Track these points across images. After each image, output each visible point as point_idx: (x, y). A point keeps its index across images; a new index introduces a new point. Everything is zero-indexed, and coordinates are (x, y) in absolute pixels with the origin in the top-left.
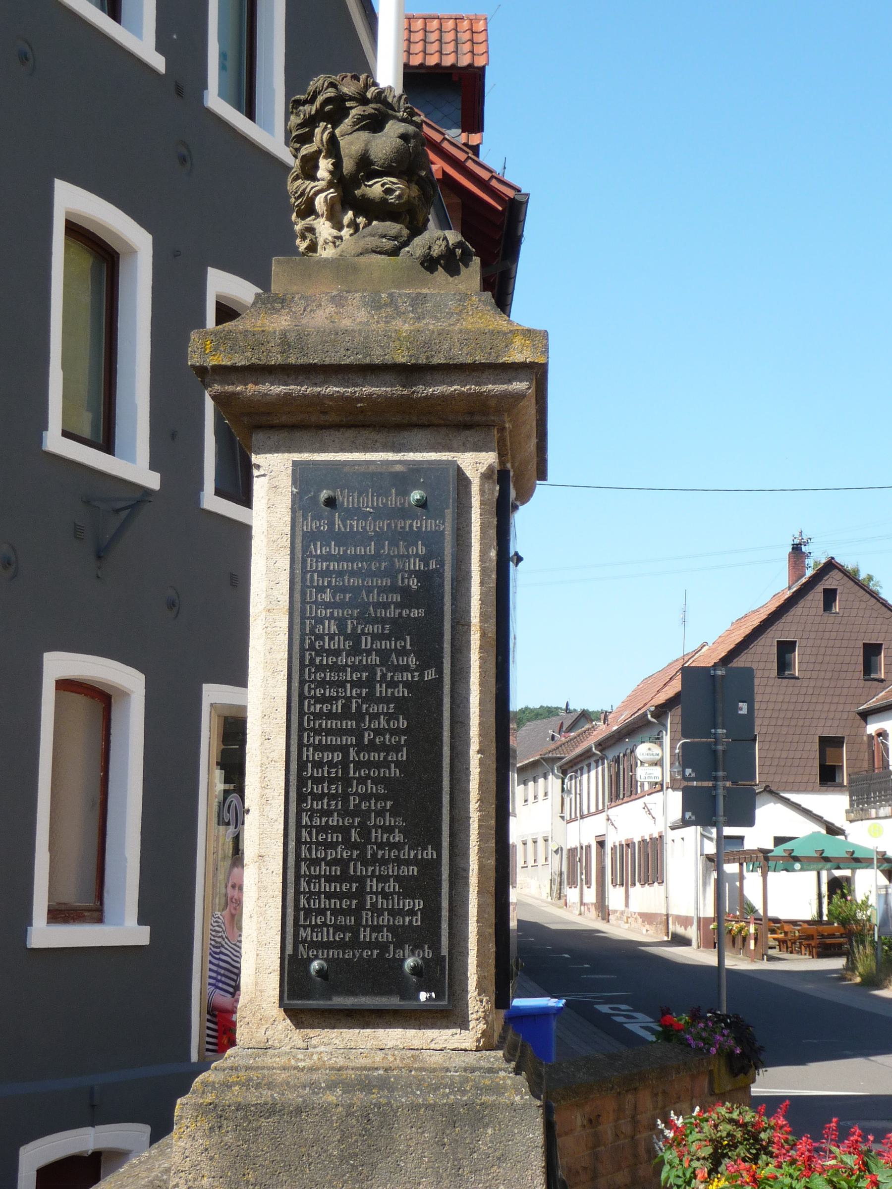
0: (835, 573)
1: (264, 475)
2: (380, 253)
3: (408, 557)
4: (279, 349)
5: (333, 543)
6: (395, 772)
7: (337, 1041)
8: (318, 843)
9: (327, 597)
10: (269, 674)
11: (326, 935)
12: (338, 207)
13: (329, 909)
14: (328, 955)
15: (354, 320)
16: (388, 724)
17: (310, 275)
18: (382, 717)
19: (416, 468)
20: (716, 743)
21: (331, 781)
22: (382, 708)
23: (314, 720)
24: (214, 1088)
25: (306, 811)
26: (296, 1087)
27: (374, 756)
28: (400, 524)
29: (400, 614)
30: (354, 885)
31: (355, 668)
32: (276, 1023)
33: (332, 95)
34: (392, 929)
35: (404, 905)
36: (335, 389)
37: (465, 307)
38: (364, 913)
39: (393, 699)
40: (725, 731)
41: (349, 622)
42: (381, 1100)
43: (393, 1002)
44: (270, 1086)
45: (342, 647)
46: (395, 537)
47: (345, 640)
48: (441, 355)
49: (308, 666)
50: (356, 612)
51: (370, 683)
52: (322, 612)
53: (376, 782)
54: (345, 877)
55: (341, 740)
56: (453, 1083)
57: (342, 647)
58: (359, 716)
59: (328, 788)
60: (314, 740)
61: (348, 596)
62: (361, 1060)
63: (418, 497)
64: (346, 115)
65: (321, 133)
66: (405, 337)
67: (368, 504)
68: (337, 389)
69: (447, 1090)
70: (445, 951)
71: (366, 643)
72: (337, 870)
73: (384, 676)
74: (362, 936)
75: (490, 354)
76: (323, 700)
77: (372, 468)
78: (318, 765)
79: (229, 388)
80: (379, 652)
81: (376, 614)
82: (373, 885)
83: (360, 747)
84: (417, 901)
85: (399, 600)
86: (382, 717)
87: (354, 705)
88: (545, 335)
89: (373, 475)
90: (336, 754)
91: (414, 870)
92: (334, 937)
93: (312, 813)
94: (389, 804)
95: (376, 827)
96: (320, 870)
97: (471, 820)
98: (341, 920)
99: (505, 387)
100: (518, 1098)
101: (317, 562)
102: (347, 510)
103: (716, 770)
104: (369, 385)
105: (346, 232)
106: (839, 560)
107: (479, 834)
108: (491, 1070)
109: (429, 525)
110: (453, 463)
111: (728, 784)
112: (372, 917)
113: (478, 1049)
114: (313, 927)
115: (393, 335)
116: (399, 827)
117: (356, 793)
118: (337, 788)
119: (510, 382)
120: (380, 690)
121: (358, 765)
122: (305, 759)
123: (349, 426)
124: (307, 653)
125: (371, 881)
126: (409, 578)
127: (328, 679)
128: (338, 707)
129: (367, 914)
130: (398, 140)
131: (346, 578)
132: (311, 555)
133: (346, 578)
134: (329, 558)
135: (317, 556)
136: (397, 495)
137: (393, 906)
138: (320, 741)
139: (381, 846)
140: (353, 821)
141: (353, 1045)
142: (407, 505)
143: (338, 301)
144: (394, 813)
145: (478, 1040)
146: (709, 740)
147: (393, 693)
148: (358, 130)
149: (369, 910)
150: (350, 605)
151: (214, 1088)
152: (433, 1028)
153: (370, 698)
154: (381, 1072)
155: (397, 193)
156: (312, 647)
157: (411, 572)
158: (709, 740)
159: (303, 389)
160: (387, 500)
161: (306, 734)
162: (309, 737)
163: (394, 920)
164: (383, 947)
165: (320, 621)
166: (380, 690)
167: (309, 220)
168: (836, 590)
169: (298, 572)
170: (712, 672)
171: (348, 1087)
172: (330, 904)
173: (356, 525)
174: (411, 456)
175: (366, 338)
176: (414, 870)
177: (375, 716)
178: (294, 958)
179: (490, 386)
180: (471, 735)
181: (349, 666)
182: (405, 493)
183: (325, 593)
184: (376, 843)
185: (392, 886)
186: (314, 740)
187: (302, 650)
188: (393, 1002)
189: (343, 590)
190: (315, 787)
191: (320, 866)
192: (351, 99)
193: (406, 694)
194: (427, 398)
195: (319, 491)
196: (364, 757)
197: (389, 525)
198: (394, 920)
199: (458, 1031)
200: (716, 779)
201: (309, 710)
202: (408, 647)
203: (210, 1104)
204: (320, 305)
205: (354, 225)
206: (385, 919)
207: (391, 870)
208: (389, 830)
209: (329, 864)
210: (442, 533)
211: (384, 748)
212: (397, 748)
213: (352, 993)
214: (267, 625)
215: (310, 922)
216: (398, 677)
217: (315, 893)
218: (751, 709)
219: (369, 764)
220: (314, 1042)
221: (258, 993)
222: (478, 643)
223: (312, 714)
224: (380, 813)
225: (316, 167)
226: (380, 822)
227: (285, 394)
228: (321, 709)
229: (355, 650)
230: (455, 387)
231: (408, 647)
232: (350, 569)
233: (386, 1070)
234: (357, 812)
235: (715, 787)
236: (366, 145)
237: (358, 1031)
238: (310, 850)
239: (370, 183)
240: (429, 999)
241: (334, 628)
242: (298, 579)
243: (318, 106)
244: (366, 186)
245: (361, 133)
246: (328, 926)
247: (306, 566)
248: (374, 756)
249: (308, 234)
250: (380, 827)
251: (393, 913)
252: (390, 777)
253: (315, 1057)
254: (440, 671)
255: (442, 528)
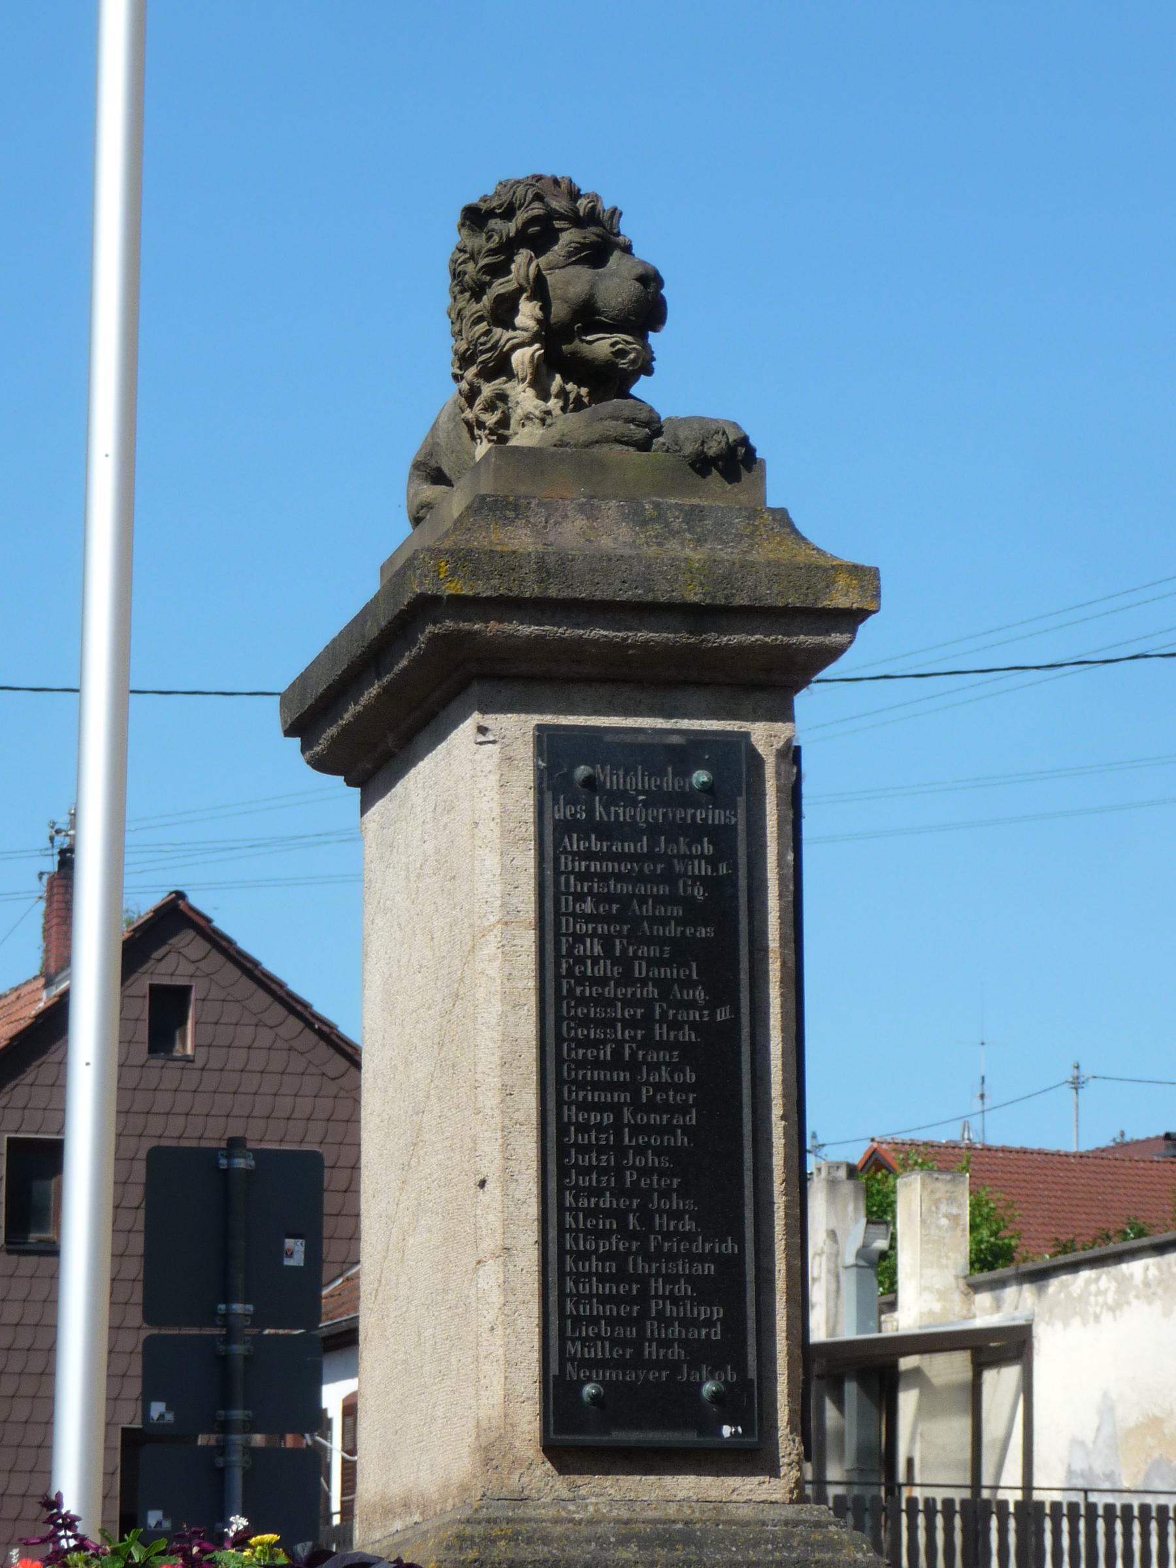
0: (186, 941)
1: (494, 742)
2: (627, 443)
3: (692, 857)
4: (534, 577)
5: (593, 837)
6: (681, 1140)
7: (612, 1491)
8: (587, 1232)
9: (588, 907)
10: (509, 1008)
11: (599, 1351)
12: (544, 369)
13: (604, 1317)
14: (604, 1376)
15: (616, 539)
16: (672, 1078)
17: (542, 472)
18: (663, 1068)
19: (699, 740)
20: (228, 1339)
21: (601, 1150)
22: (664, 1056)
23: (576, 1070)
24: (473, 1543)
25: (570, 1189)
26: (578, 1542)
27: (654, 1119)
28: (680, 813)
29: (683, 932)
30: (635, 1287)
31: (627, 1003)
32: (533, 1467)
33: (541, 212)
34: (684, 1343)
35: (699, 1314)
36: (602, 632)
37: (756, 528)
38: (649, 1323)
39: (675, 1045)
40: (250, 1307)
41: (618, 942)
42: (690, 1557)
43: (690, 1437)
44: (545, 1540)
45: (609, 974)
46: (673, 830)
47: (613, 965)
48: (744, 594)
49: (566, 997)
50: (625, 928)
51: (647, 1022)
52: (582, 928)
53: (659, 1152)
54: (621, 1276)
55: (612, 1097)
56: (775, 1538)
57: (609, 974)
58: (634, 1066)
59: (598, 1159)
60: (577, 1095)
61: (615, 907)
62: (650, 1513)
63: (706, 779)
64: (555, 240)
65: (522, 264)
66: (698, 569)
67: (639, 781)
68: (605, 633)
69: (770, 1547)
70: (752, 1374)
71: (640, 970)
72: (611, 1267)
73: (664, 1014)
74: (646, 1353)
75: (806, 595)
76: (586, 1043)
77: (641, 738)
78: (583, 1128)
79: (465, 626)
80: (657, 982)
81: (651, 932)
82: (658, 1286)
83: (637, 1106)
84: (715, 1309)
85: (681, 913)
86: (663, 1068)
87: (627, 1052)
88: (874, 573)
89: (643, 747)
90: (605, 1116)
91: (710, 1268)
92: (611, 1353)
93: (578, 1191)
94: (676, 1181)
95: (660, 1211)
96: (590, 1266)
97: (776, 1206)
98: (620, 1331)
99: (819, 639)
100: (859, 1556)
101: (573, 861)
102: (611, 793)
103: (227, 1403)
104: (646, 629)
105: (554, 404)
106: (198, 900)
107: (786, 1225)
108: (818, 1525)
109: (717, 817)
110: (747, 735)
111: (258, 1439)
112: (659, 1328)
113: (792, 1502)
114: (584, 1340)
115: (683, 564)
116: (689, 1212)
117: (633, 1167)
118: (608, 1160)
119: (827, 632)
120: (660, 1032)
121: (636, 1130)
122: (566, 1119)
123: (604, 681)
124: (564, 982)
125: (656, 1282)
126: (693, 885)
127: (592, 1015)
128: (607, 1053)
129: (652, 1325)
130: (637, 285)
131: (612, 883)
132: (565, 852)
133: (612, 883)
134: (588, 855)
135: (573, 853)
136: (674, 775)
137: (685, 1314)
138: (585, 1097)
139: (668, 1236)
140: (631, 1203)
141: (633, 1495)
142: (687, 790)
143: (589, 511)
144: (683, 1194)
145: (791, 1492)
146: (207, 1331)
147: (676, 1037)
148: (573, 263)
149: (654, 1319)
150: (619, 919)
151: (473, 1543)
152: (733, 1475)
153: (648, 1043)
154: (680, 1526)
155: (632, 356)
156: (570, 973)
157: (696, 879)
158: (207, 1331)
159: (561, 630)
160: (662, 782)
161: (566, 1088)
162: (570, 1092)
163: (687, 1332)
164: (675, 1367)
165: (579, 939)
166: (660, 1032)
167: (498, 383)
168: (186, 990)
169: (549, 873)
170: (223, 1162)
171: (645, 1542)
172: (604, 1312)
173: (622, 813)
174: (685, 724)
175: (648, 567)
176: (710, 1268)
177: (655, 1067)
178: (560, 1378)
179: (802, 637)
180: (773, 1095)
181: (619, 1000)
182: (684, 773)
183: (585, 902)
184: (660, 1232)
185: (683, 1289)
186: (577, 1095)
187: (558, 977)
188: (690, 1437)
189: (609, 898)
190: (580, 1158)
191: (590, 1260)
192: (562, 217)
193: (693, 1039)
194: (720, 648)
195: (573, 767)
196: (642, 1120)
197: (665, 815)
198: (687, 1332)
199: (767, 1478)
200: (225, 1427)
201: (569, 1055)
202: (695, 977)
203: (475, 1561)
204: (566, 516)
205: (563, 394)
206: (676, 1330)
207: (681, 1267)
208: (677, 1215)
209: (602, 1258)
210: (734, 828)
211: (666, 1108)
212: (684, 1109)
213: (638, 1427)
214: (504, 942)
215: (580, 1333)
216: (682, 1016)
217: (585, 1296)
218: (314, 1255)
219: (648, 1129)
220: (583, 1491)
221: (509, 1428)
222: (778, 974)
223: (573, 1061)
224: (665, 1194)
225: (515, 311)
226: (665, 1204)
227: (537, 636)
228: (585, 1054)
229: (627, 979)
230: (757, 636)
231: (695, 977)
232: (616, 871)
233: (686, 1523)
234: (635, 1191)
235: (222, 1449)
236: (592, 287)
237: (638, 1477)
238: (576, 1240)
239: (589, 338)
240: (734, 1435)
241: (598, 949)
242: (549, 883)
243: (520, 225)
244: (583, 341)
245: (578, 268)
246: (603, 1339)
247: (559, 866)
248: (654, 1119)
249: (499, 404)
250: (666, 1211)
251: (686, 1323)
252: (676, 1147)
253: (591, 1509)
254: (736, 1010)
255: (733, 820)
